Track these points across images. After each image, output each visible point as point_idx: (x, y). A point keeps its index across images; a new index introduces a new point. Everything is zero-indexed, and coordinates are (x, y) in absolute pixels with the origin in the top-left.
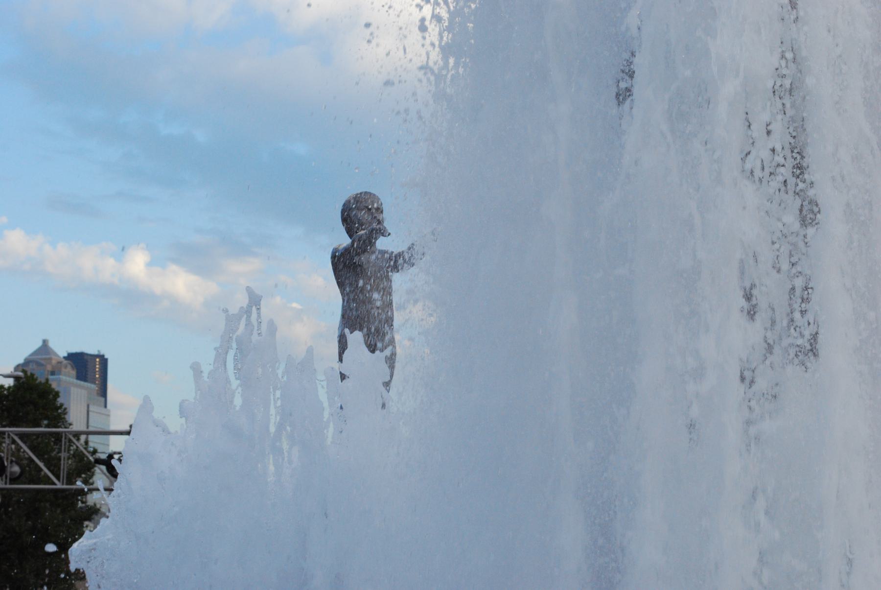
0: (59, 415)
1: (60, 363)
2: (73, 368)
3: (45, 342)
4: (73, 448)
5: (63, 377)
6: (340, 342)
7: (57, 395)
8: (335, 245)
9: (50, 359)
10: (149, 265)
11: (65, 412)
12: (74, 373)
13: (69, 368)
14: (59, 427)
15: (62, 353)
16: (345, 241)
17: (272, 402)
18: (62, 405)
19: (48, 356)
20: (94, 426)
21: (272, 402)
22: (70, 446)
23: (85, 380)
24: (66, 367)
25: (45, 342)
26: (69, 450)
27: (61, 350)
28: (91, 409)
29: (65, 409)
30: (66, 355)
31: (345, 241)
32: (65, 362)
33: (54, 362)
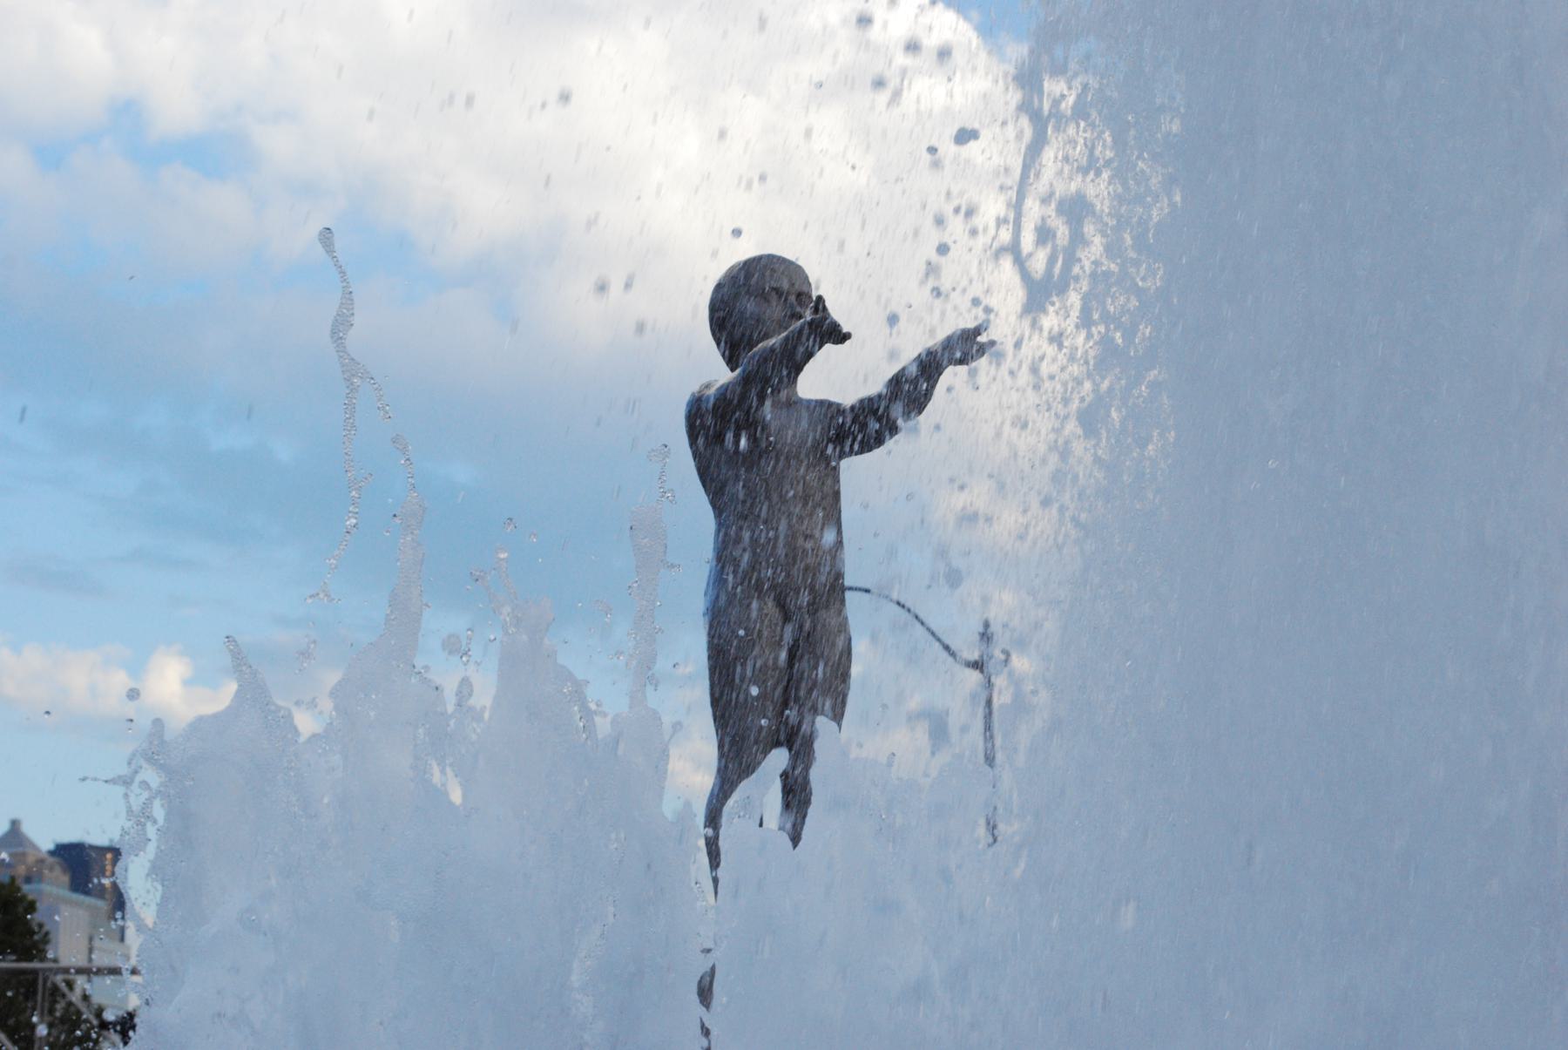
0: (35, 945)
1: (41, 861)
2: (64, 871)
3: (15, 824)
4: (60, 1006)
5: (47, 888)
6: (718, 854)
7: (31, 907)
8: (694, 387)
9: (24, 854)
10: (187, 683)
11: (46, 939)
12: (66, 879)
13: (58, 871)
14: (31, 960)
15: (45, 843)
16: (718, 373)
17: (782, 537)
18: (41, 926)
19: (20, 850)
20: (100, 959)
21: (782, 537)
22: (55, 1002)
23: (87, 893)
24: (51, 869)
25: (15, 824)
26: (51, 1011)
27: (44, 837)
28: (97, 943)
29: (47, 934)
30: (51, 847)
31: (718, 373)
32: (51, 860)
33: (31, 859)
